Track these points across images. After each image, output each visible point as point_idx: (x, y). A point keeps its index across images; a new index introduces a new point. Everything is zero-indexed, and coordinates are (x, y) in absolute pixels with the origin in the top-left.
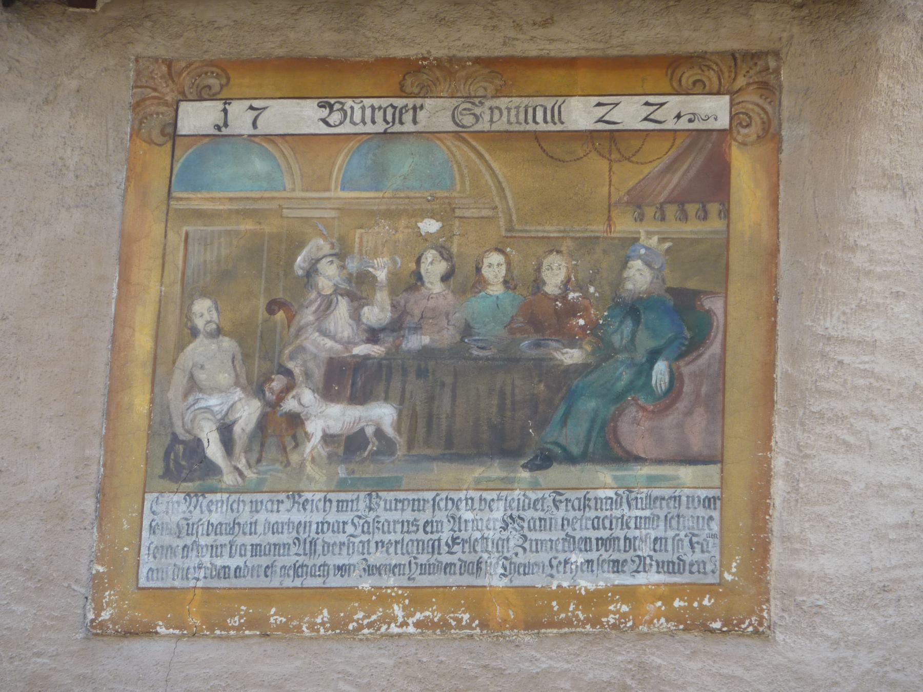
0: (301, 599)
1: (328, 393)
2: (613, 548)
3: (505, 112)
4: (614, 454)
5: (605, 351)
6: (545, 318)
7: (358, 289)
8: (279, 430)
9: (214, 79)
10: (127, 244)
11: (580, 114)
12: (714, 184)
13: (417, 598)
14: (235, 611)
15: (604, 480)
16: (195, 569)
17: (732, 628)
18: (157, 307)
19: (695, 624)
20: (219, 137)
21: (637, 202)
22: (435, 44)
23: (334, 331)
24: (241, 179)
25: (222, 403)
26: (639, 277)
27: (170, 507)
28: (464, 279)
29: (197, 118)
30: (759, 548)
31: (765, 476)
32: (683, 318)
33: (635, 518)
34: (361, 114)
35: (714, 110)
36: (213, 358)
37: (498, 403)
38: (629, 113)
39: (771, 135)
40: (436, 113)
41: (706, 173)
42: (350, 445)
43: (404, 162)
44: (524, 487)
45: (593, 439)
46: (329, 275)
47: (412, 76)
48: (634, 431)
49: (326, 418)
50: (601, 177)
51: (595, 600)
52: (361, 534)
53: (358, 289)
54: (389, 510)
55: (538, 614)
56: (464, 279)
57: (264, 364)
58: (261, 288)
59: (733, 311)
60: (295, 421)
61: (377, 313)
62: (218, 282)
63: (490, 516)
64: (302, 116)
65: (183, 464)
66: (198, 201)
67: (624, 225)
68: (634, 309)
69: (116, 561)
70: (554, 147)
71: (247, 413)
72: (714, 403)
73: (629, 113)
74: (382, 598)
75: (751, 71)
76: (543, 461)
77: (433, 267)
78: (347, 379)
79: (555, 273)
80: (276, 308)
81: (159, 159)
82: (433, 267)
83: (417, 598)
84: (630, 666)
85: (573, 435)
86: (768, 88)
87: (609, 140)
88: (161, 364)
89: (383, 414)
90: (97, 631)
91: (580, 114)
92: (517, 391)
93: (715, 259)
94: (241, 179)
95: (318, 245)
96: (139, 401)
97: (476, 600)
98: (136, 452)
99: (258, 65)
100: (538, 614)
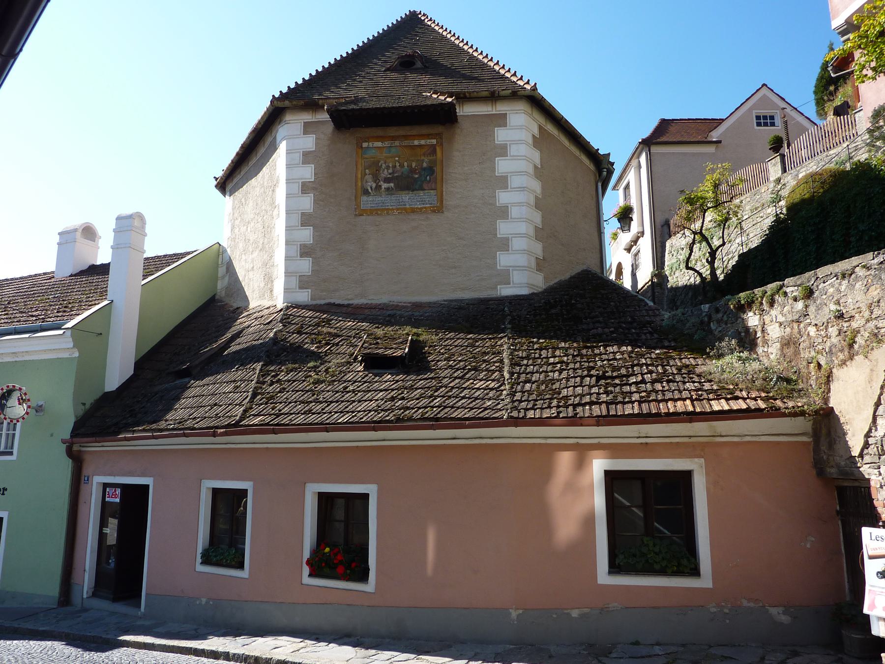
0: (383, 210)
1: (385, 182)
2: (423, 202)
5: (421, 176)
6: (412, 171)
7: (388, 168)
8: (378, 187)
9: (367, 140)
10: (357, 162)
11: (416, 143)
12: (434, 152)
13: (398, 209)
14: (372, 212)
15: (421, 193)
16: (368, 206)
17: (439, 212)
19: (434, 211)
20: (368, 148)
21: (424, 155)
22: (397, 134)
23: (385, 174)
24: (372, 153)
25: (371, 184)
26: (425, 165)
27: (364, 198)
28: (402, 166)
29: (365, 145)
30: (442, 202)
31: (442, 192)
32: (431, 170)
33: (427, 197)
34: (387, 144)
35: (434, 141)
37: (411, 181)
38: (423, 142)
39: (442, 145)
40: (397, 143)
41: (433, 150)
42: (388, 189)
43: (393, 150)
44: (411, 194)
45: (742, 405)
46: (384, 166)
47: (393, 138)
48: (425, 186)
49: (385, 186)
51: (421, 208)
52: (390, 201)
53: (388, 168)
54: (393, 198)
55: (413, 211)
56: (402, 166)
57: (376, 178)
58: (375, 168)
59: (438, 169)
60: (380, 186)
61: (390, 171)
62: (369, 167)
63: (406, 198)
65: (366, 192)
66: (365, 156)
67: (423, 158)
68: (424, 169)
69: (358, 206)
70: (414, 147)
71: (374, 185)
73: (423, 142)
74: (393, 209)
75: (438, 136)
76: (413, 191)
77: (398, 164)
78: (387, 180)
79: (414, 165)
81: (360, 151)
82: (398, 164)
83: (398, 209)
85: (417, 187)
86: (441, 138)
87: (420, 146)
88: (362, 179)
89: (392, 185)
90: (356, 215)
91: (416, 143)
92: (718, 272)
93: (435, 162)
94: (372, 153)
95: (382, 162)
96: (360, 184)
97: (405, 209)
98: (360, 191)
99: (373, 137)
100: (413, 211)
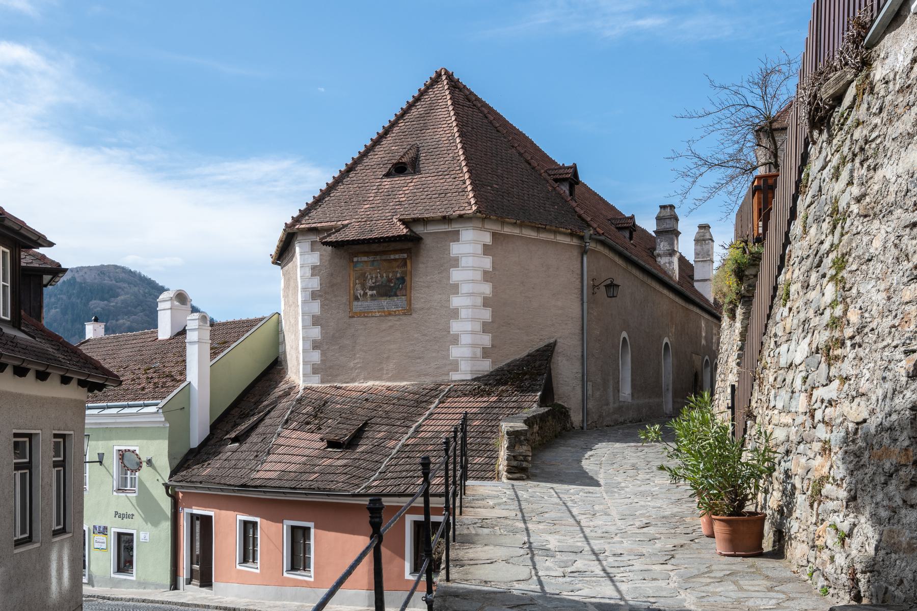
2: (397, 306)
3: (384, 257)
4: (396, 296)
6: (390, 281)
8: (365, 294)
11: (392, 257)
12: (405, 264)
18: (580, 323)
19: (405, 314)
20: (357, 262)
21: (398, 267)
23: (370, 283)
26: (398, 275)
27: (355, 303)
28: (382, 277)
29: (355, 259)
32: (402, 280)
34: (371, 258)
35: (405, 255)
36: (358, 286)
38: (397, 256)
40: (378, 258)
42: (372, 296)
43: (375, 263)
48: (398, 293)
49: (370, 293)
50: (395, 264)
53: (372, 278)
54: (376, 302)
56: (382, 277)
57: (363, 288)
58: (363, 277)
59: (407, 279)
63: (385, 302)
64: (365, 259)
65: (357, 299)
68: (398, 279)
69: (351, 310)
70: (390, 261)
71: (362, 293)
72: (406, 289)
73: (397, 256)
78: (371, 288)
80: (78, 326)
84: (651, 530)
87: (395, 260)
88: (354, 286)
91: (392, 257)
